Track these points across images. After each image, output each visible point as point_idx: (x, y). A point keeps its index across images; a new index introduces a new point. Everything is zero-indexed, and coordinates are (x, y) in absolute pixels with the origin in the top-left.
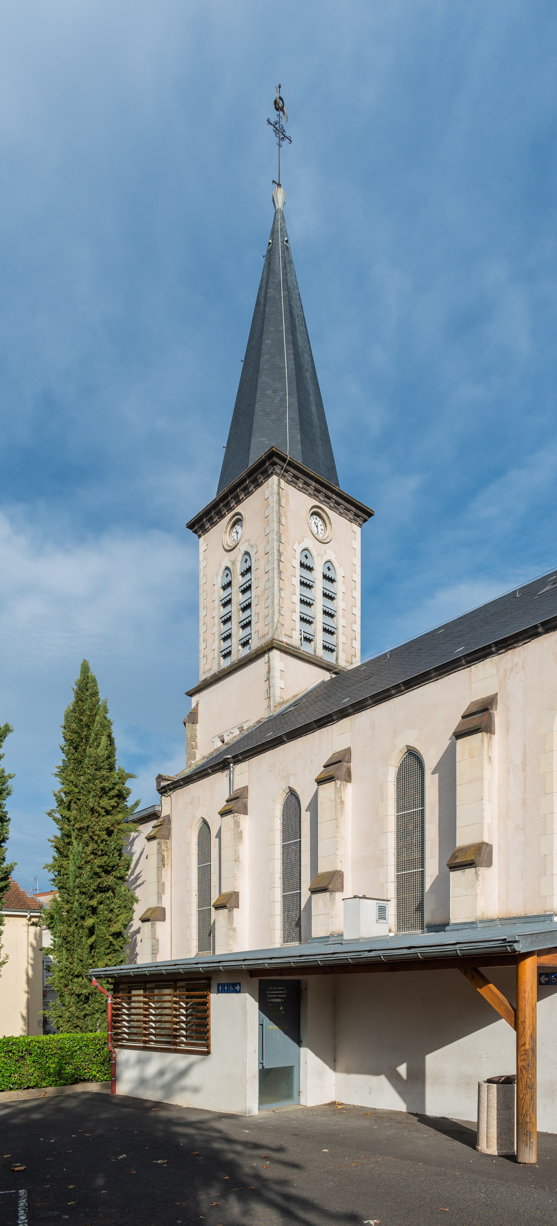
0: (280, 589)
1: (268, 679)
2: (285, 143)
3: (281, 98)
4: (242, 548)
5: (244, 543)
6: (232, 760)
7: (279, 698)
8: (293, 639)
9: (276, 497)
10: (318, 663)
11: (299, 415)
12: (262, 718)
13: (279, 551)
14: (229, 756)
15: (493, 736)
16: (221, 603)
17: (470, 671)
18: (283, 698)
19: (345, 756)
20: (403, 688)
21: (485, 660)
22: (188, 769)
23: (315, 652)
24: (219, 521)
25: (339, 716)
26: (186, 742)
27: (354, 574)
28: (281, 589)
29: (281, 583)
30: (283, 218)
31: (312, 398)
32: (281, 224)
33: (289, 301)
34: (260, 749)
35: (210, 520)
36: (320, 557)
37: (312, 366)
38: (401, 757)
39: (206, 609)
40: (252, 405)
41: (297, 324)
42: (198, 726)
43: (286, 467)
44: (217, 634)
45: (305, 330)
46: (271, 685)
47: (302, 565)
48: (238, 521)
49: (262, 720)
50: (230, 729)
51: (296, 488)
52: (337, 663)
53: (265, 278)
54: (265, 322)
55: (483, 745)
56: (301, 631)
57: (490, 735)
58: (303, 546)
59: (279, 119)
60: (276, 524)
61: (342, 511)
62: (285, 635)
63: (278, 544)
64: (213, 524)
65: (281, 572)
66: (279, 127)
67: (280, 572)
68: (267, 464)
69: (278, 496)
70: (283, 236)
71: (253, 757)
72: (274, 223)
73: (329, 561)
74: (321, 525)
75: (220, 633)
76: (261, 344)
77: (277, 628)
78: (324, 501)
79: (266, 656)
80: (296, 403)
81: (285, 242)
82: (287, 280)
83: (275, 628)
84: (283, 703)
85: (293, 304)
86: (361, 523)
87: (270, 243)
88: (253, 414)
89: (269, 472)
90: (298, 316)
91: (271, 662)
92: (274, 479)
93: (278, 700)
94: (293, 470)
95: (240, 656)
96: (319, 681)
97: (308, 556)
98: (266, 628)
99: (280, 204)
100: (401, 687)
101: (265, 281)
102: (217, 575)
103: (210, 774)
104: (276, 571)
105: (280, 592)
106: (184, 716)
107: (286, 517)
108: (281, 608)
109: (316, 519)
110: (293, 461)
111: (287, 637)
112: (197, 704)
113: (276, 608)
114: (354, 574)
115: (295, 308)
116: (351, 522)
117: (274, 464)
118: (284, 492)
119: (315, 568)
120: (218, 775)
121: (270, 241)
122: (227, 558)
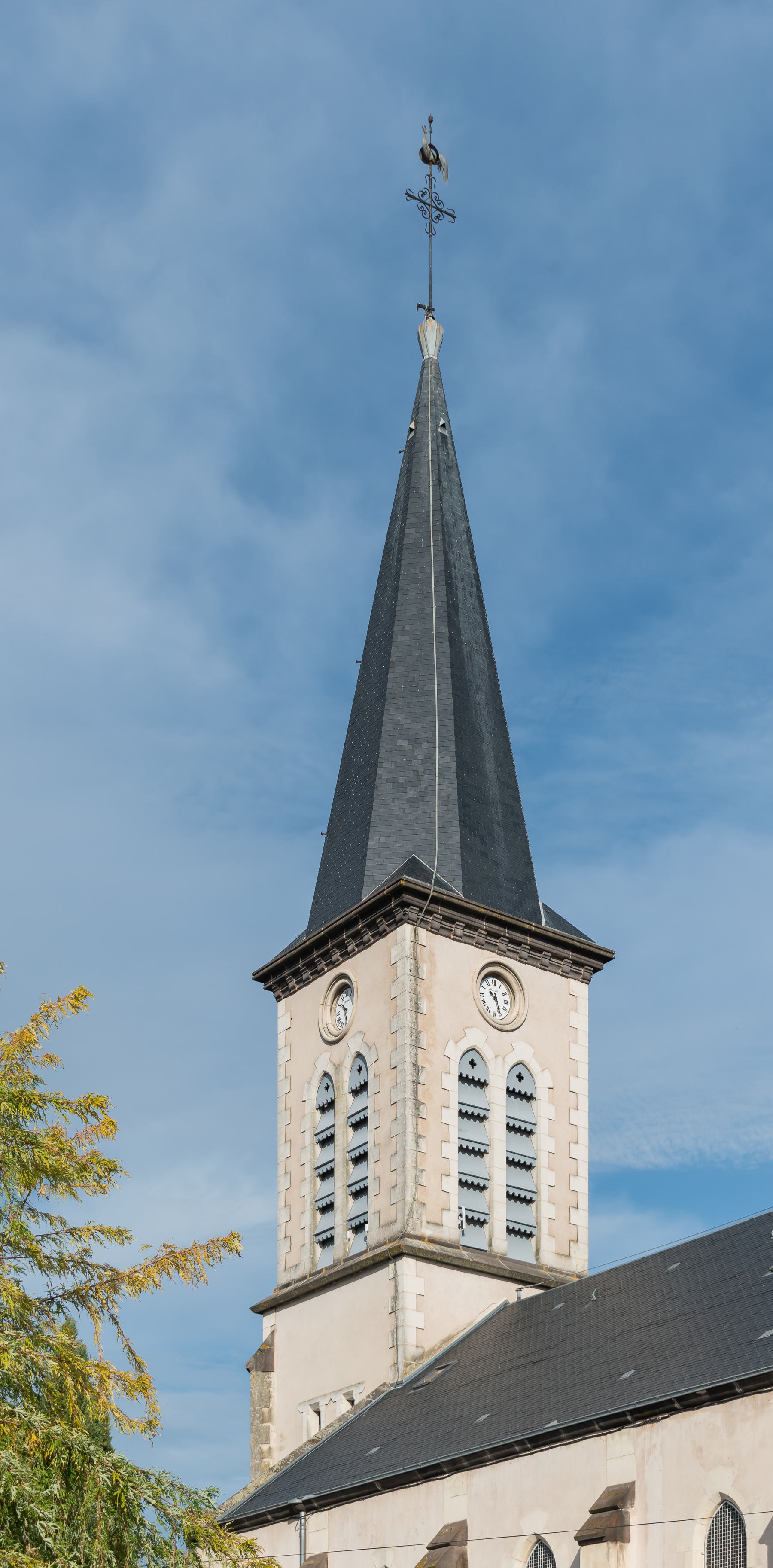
0: (418, 1137)
1: (394, 1311)
2: (443, 225)
3: (431, 146)
4: (352, 1044)
5: (355, 1035)
6: (302, 1506)
7: (414, 1348)
8: (444, 1228)
9: (409, 964)
10: (494, 1271)
11: (459, 790)
12: (384, 1385)
13: (415, 1065)
14: (297, 1501)
15: (626, 1544)
16: (315, 1139)
17: (606, 1441)
18: (422, 1347)
19: (456, 1535)
20: (529, 1446)
21: (623, 1430)
22: (241, 1494)
23: (490, 1245)
24: (313, 980)
25: (450, 1468)
26: (252, 1409)
27: (573, 1079)
28: (420, 1136)
29: (420, 1126)
30: (438, 379)
31: (488, 746)
32: (432, 393)
33: (445, 554)
34: (344, 1496)
35: (296, 974)
36: (500, 1059)
37: (489, 676)
38: (529, 1548)
39: (289, 1144)
40: (372, 765)
41: (460, 596)
42: (274, 1377)
43: (428, 906)
44: (308, 1199)
45: (477, 604)
46: (400, 1324)
47: (463, 1079)
48: (344, 988)
49: (384, 1389)
50: (330, 1393)
51: (449, 937)
52: (537, 1260)
53: (402, 498)
54: (399, 598)
55: (608, 1560)
56: (460, 1208)
57: (622, 1544)
58: (464, 1046)
59: (431, 183)
60: (409, 1016)
61: (546, 961)
62: (428, 1222)
63: (413, 1052)
64: (306, 983)
65: (420, 1103)
66: (431, 197)
67: (418, 1104)
68: (393, 904)
69: (413, 961)
70: (436, 418)
71: (335, 1507)
72: (420, 388)
73: (521, 1063)
74: (504, 994)
75: (315, 1197)
76: (390, 643)
77: (411, 1212)
78: (508, 950)
79: (391, 1266)
80: (453, 767)
81: (440, 430)
82: (442, 508)
83: (407, 1212)
84: (422, 1356)
85: (452, 557)
86: (587, 975)
87: (411, 430)
88: (372, 787)
89: (398, 918)
90: (462, 580)
91: (399, 1279)
92: (406, 930)
93: (412, 1351)
94: (444, 909)
95: (349, 1251)
96: (495, 1304)
97: (475, 1061)
98: (393, 1210)
99: (431, 351)
100: (526, 1444)
101: (400, 507)
102: (309, 1083)
103: (271, 1521)
104: (410, 1104)
105: (417, 1143)
106: (247, 1356)
107: (430, 997)
108: (419, 1172)
109: (494, 984)
110: (441, 896)
111: (431, 1226)
112: (273, 1333)
113: (410, 1174)
114: (573, 1079)
115: (457, 563)
116: (567, 977)
117: (405, 905)
118: (425, 949)
119: (491, 1081)
120: (283, 1525)
121: (412, 426)
122: (326, 1056)
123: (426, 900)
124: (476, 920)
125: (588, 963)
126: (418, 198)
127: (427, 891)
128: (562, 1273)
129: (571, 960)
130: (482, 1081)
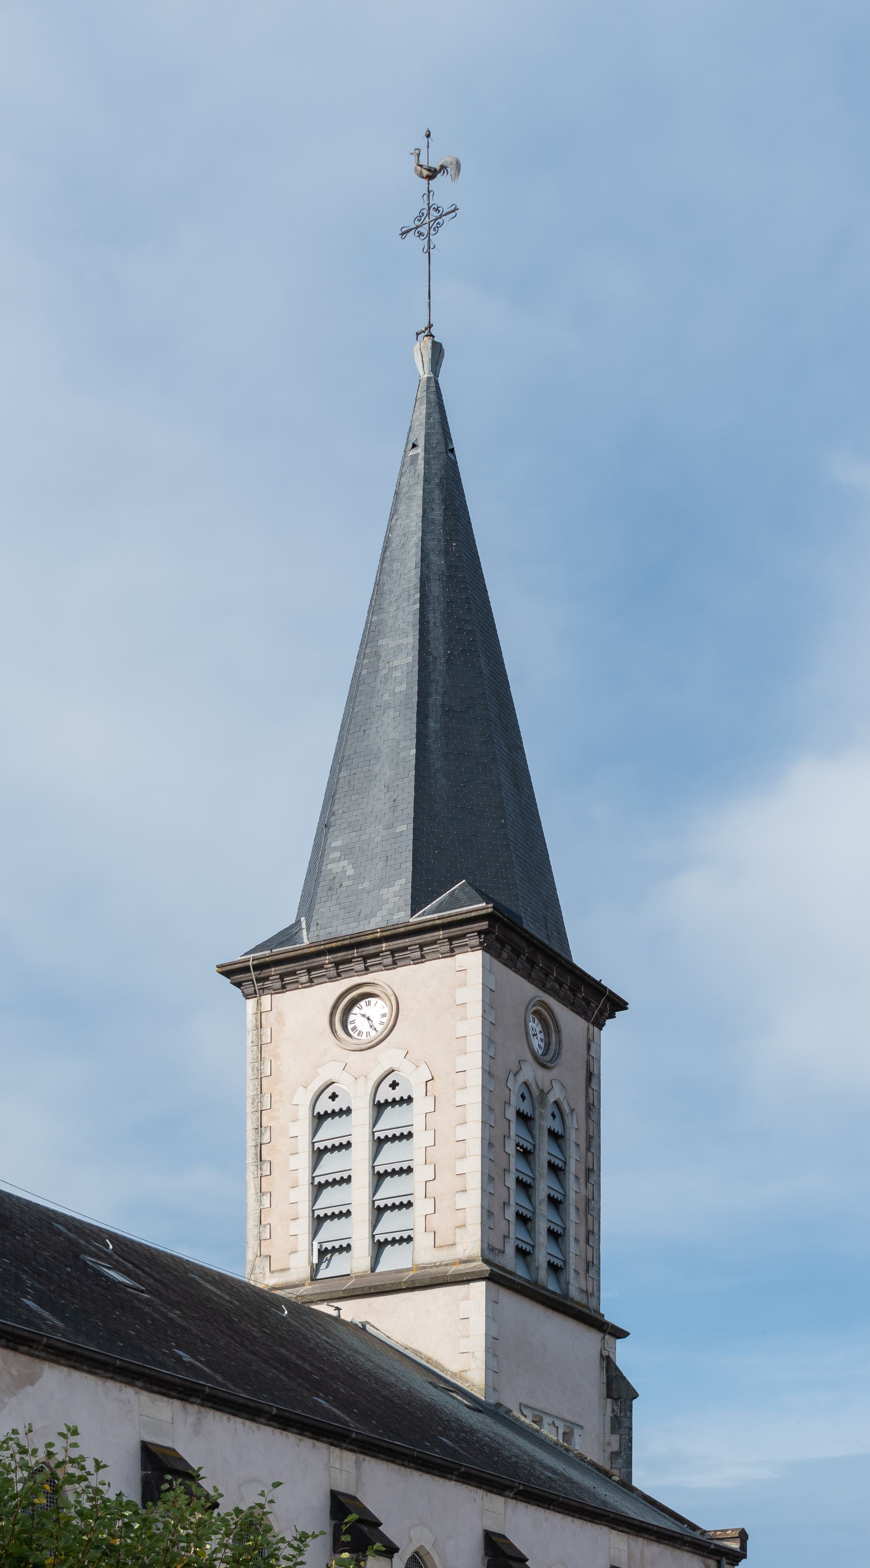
123: (250, 972)
124: (318, 959)
125: (469, 931)
126: (427, 238)
127: (246, 964)
128: (439, 1266)
129: (444, 939)
130: (405, 1097)
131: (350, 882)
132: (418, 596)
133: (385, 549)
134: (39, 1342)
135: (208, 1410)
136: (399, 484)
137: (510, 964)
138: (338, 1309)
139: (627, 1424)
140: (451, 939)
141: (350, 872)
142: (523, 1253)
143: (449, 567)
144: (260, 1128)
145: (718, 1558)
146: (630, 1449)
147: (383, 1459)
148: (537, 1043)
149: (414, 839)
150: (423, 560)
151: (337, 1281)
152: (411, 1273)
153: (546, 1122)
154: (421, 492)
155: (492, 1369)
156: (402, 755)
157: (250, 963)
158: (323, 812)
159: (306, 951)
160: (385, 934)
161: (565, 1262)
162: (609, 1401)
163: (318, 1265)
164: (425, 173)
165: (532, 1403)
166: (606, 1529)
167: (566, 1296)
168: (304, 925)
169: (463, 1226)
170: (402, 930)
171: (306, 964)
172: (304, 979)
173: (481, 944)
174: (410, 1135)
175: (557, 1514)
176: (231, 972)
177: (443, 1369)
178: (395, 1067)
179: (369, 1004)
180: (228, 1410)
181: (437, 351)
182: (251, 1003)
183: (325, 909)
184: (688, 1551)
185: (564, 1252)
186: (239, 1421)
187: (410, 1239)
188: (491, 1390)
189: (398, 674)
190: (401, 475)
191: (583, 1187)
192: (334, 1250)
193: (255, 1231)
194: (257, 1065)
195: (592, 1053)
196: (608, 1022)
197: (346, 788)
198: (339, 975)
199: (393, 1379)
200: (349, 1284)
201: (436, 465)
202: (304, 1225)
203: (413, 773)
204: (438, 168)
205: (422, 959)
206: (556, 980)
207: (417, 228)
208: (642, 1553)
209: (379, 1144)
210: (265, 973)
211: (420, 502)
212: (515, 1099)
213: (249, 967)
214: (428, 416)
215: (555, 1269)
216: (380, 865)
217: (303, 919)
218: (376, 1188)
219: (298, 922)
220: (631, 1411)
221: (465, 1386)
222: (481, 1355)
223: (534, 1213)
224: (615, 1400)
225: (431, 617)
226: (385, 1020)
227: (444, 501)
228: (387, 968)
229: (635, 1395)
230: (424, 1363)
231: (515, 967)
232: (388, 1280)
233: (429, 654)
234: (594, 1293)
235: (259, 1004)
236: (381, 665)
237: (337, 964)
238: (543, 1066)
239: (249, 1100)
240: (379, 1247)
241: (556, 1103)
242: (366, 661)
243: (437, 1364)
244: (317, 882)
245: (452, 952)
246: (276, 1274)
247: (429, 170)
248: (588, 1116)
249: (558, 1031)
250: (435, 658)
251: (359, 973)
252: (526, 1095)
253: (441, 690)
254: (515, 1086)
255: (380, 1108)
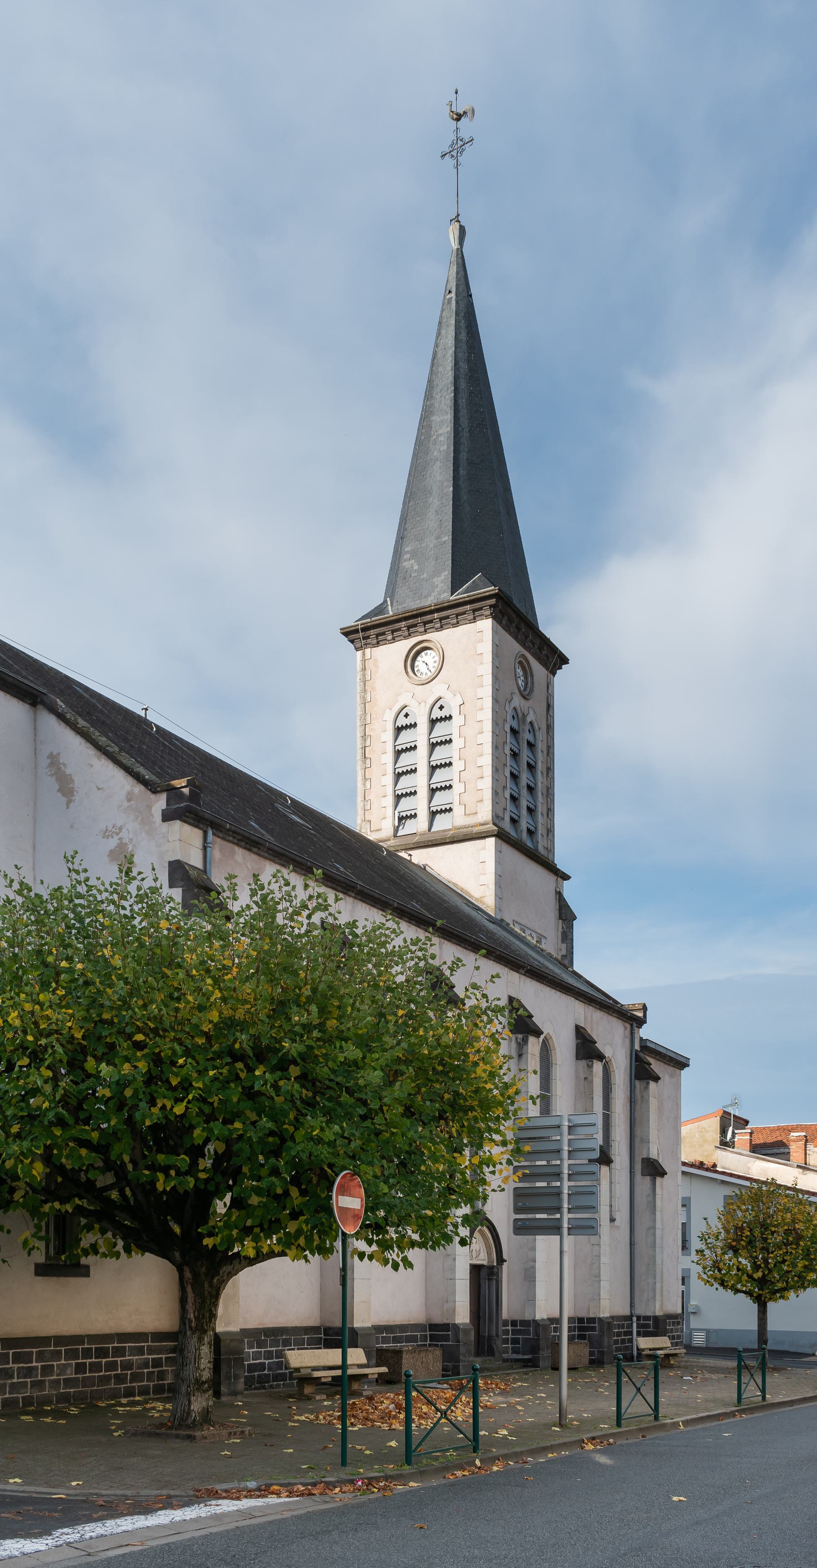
130: (448, 716)
131: (416, 574)
132: (453, 388)
133: (434, 358)
134: (264, 846)
135: (358, 901)
136: (441, 317)
137: (507, 629)
138: (410, 855)
139: (570, 937)
140: (474, 611)
141: (416, 567)
142: (514, 821)
143: (470, 370)
144: (364, 736)
145: (631, 1022)
146: (572, 953)
147: (454, 943)
148: (521, 682)
149: (452, 546)
150: (455, 365)
151: (409, 838)
152: (452, 832)
153: (527, 736)
154: (454, 322)
155: (499, 897)
156: (445, 491)
157: (359, 627)
158: (399, 530)
159: (391, 619)
160: (436, 607)
161: (536, 828)
162: (560, 921)
163: (398, 827)
164: (455, 116)
165: (520, 921)
166: (573, 999)
167: (537, 850)
168: (389, 603)
169: (482, 801)
170: (446, 604)
171: (391, 627)
172: (390, 637)
173: (491, 614)
174: (450, 741)
175: (547, 988)
176: (349, 633)
177: (471, 896)
178: (442, 695)
179: (426, 654)
180: (370, 902)
181: (462, 230)
182: (359, 653)
183: (402, 591)
184: (615, 1017)
185: (535, 822)
186: (375, 910)
187: (450, 810)
188: (498, 910)
189: (442, 438)
190: (442, 311)
191: (545, 779)
192: (407, 817)
193: (362, 804)
194: (363, 694)
195: (550, 691)
196: (558, 671)
197: (413, 513)
198: (410, 635)
199: (446, 899)
200: (416, 839)
201: (462, 305)
202: (390, 800)
203: (451, 502)
204: (462, 113)
205: (457, 624)
206: (532, 642)
207: (450, 152)
208: (592, 1016)
209: (433, 746)
210: (368, 633)
211: (453, 328)
212: (509, 718)
213: (358, 629)
214: (458, 273)
215: (530, 833)
216: (433, 563)
217: (388, 599)
218: (431, 776)
219: (385, 601)
220: (572, 928)
221: (483, 907)
222: (492, 886)
223: (519, 795)
224: (564, 920)
225: (460, 402)
226: (436, 665)
227: (467, 327)
228: (438, 630)
229: (575, 918)
230: (459, 891)
231: (509, 630)
232: (437, 837)
233: (460, 426)
234: (551, 850)
235: (364, 654)
236: (432, 433)
237: (409, 627)
238: (524, 698)
239: (358, 718)
240: (433, 814)
241: (531, 723)
242: (423, 431)
243: (467, 893)
244: (397, 575)
245: (474, 620)
246: (374, 833)
247: (457, 114)
248: (548, 733)
249: (532, 676)
250: (463, 429)
251: (422, 634)
252: (515, 716)
253: (466, 450)
254: (509, 709)
255: (433, 722)
